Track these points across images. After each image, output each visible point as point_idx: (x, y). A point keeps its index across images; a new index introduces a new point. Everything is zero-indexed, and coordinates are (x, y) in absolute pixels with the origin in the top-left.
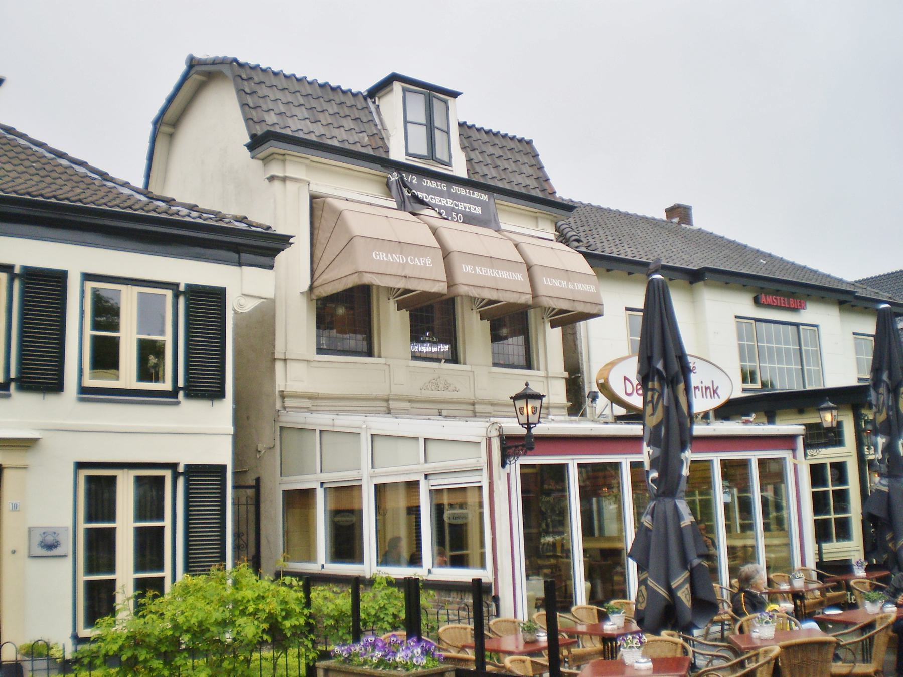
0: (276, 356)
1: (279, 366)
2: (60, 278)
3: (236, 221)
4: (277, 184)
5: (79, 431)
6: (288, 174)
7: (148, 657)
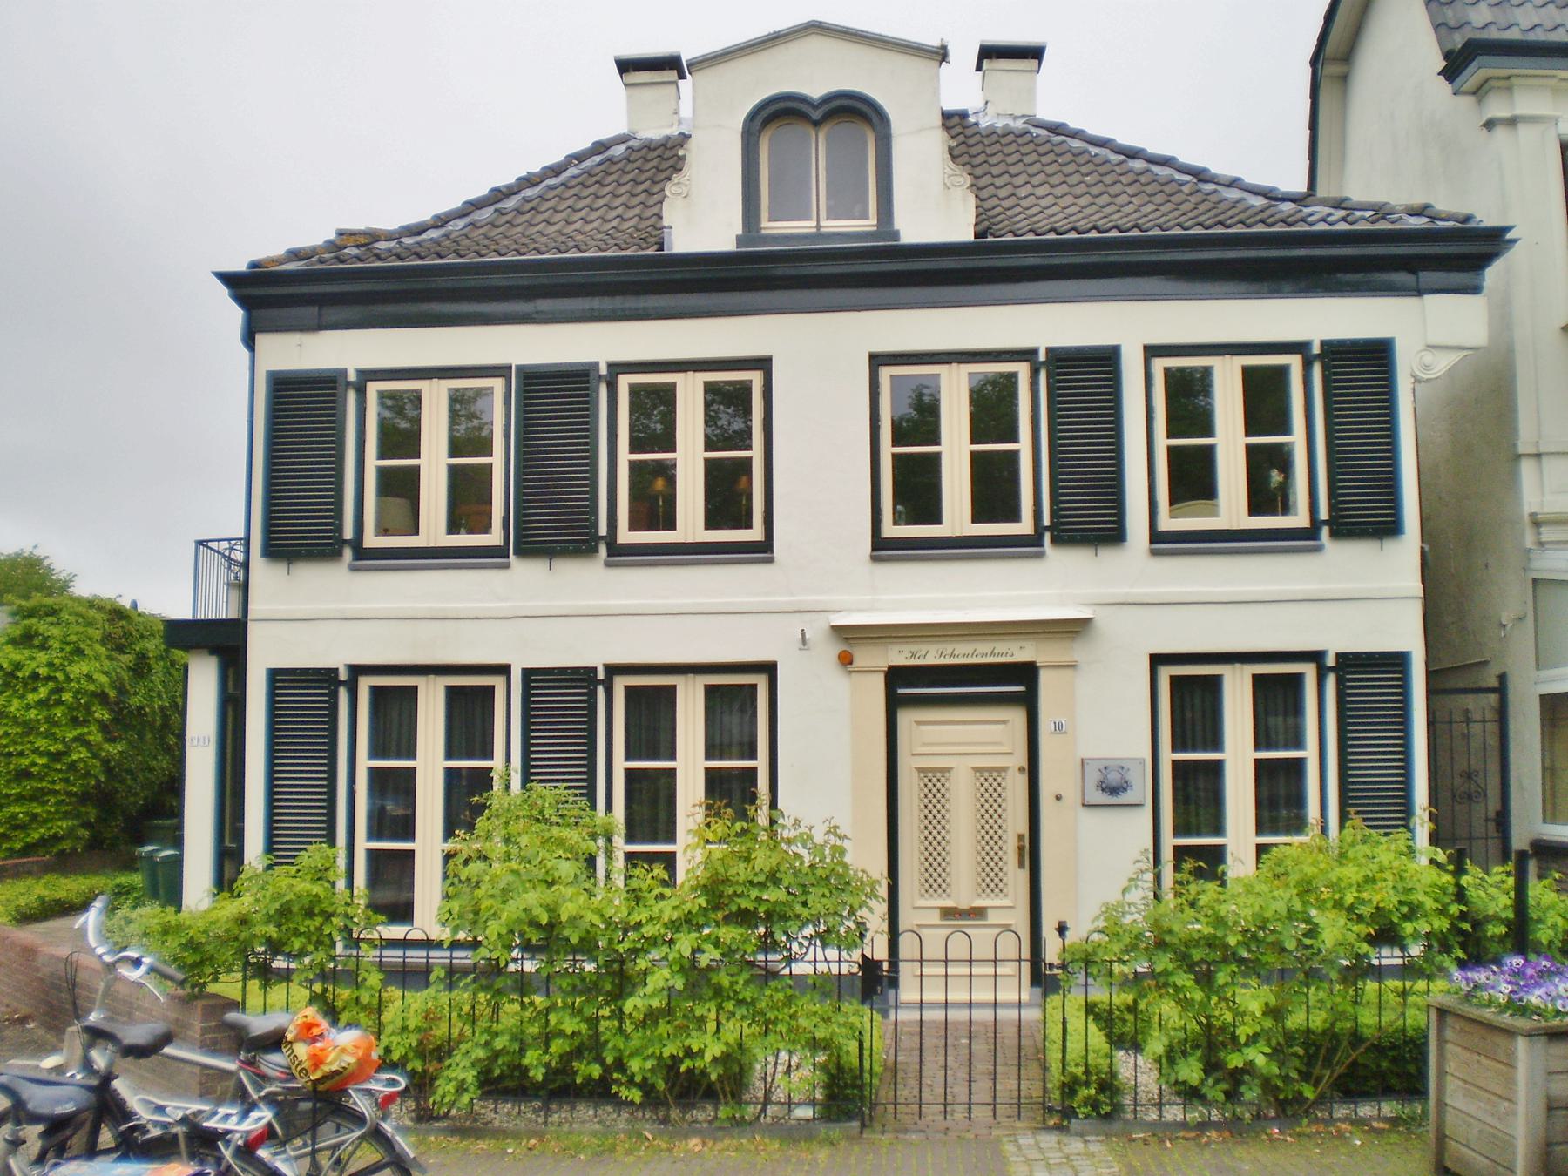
0: (1521, 449)
1: (1527, 469)
2: (1109, 359)
3: (1411, 215)
4: (1500, 133)
5: (1375, 599)
6: (1518, 111)
7: (1170, 967)
